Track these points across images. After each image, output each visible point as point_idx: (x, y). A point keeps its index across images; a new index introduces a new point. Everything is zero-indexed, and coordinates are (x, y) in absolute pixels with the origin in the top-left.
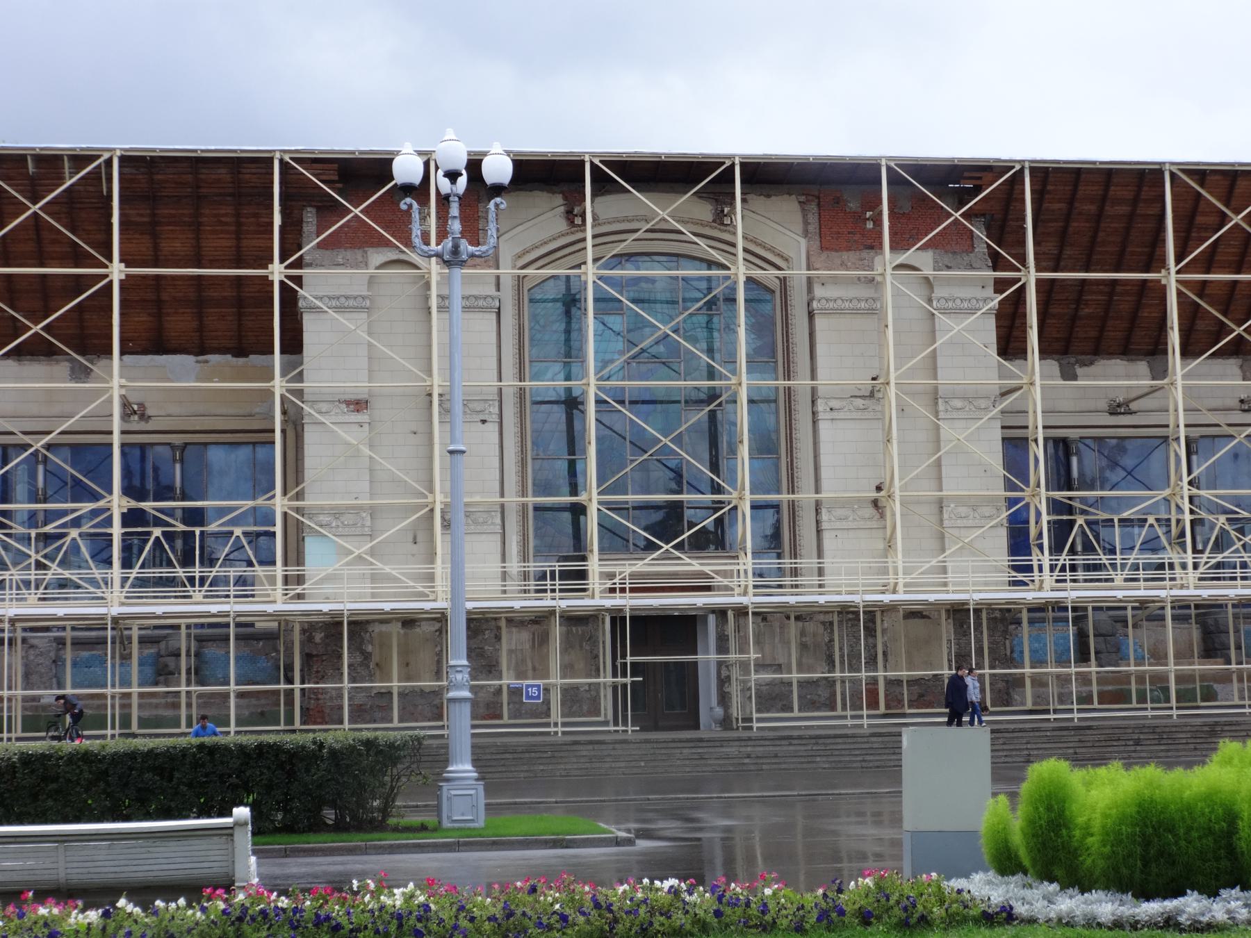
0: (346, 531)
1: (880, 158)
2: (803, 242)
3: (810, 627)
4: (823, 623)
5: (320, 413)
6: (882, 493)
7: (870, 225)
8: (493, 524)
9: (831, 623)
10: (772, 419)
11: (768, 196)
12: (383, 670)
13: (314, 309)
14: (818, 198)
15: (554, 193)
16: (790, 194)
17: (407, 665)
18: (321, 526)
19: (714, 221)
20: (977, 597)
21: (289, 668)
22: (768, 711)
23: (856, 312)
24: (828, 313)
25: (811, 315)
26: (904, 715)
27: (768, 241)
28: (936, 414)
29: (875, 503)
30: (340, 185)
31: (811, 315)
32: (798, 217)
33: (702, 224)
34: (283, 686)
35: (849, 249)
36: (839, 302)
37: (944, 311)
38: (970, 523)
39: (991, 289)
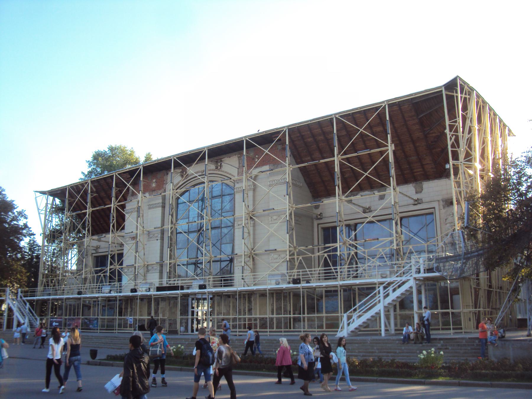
1: (242, 138)
11: (230, 157)
12: (322, 312)
21: (290, 312)
27: (229, 172)
33: (213, 170)
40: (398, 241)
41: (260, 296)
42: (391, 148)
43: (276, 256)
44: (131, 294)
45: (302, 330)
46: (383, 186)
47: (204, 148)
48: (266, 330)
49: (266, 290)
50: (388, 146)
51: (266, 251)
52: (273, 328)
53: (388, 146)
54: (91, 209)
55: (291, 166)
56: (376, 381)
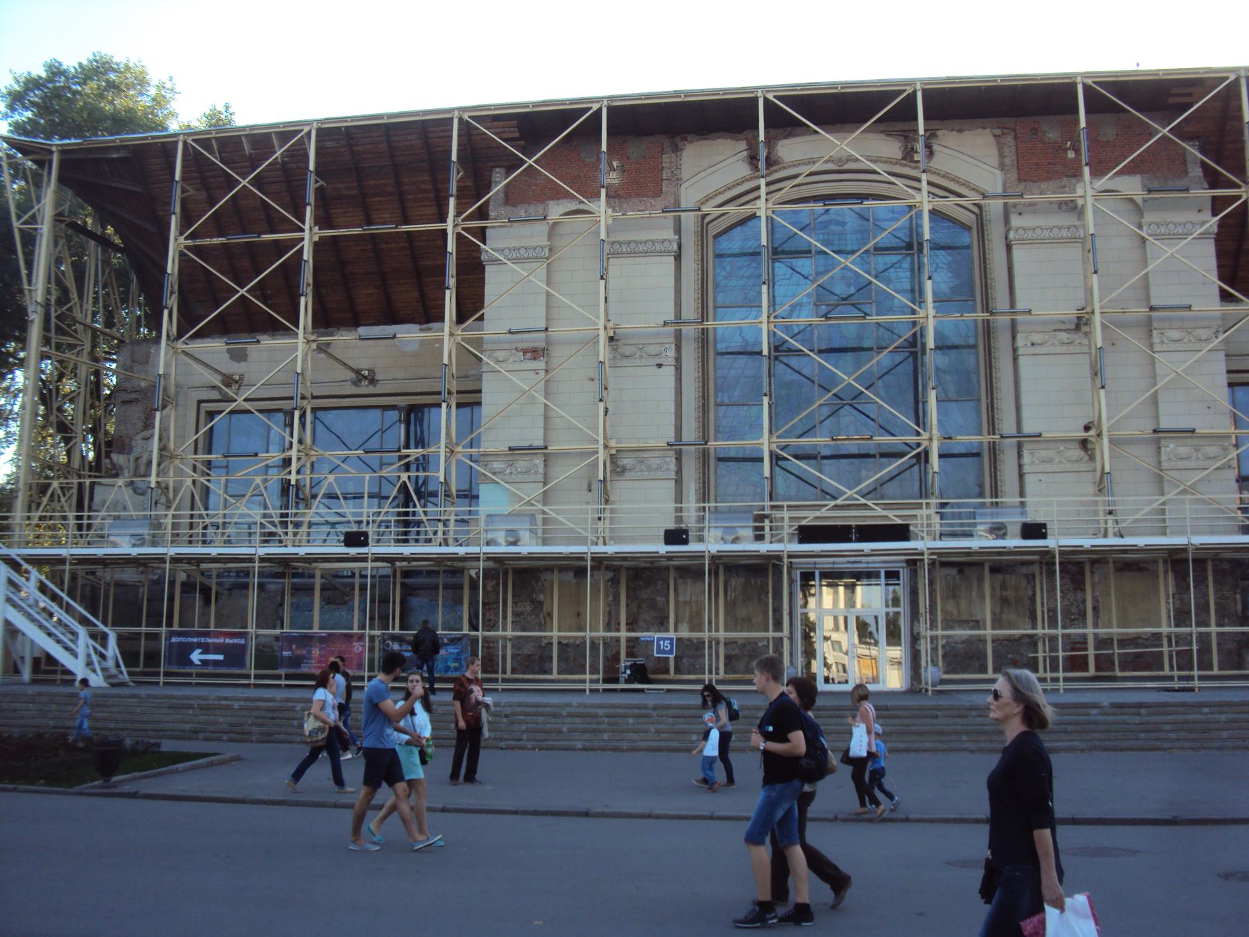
0: (520, 478)
1: (1075, 75)
2: (998, 173)
3: (1012, 580)
4: (1026, 576)
5: (497, 361)
6: (1092, 432)
7: (1071, 154)
8: (668, 470)
9: (1034, 575)
10: (972, 359)
11: (960, 131)
13: (496, 261)
14: (1014, 130)
15: (737, 140)
16: (985, 128)
17: (579, 615)
18: (494, 474)
19: (903, 158)
20: (1197, 540)
22: (964, 672)
23: (1059, 241)
24: (1023, 242)
25: (1009, 248)
26: (1114, 679)
27: (963, 176)
28: (1151, 346)
29: (1084, 443)
30: (523, 143)
31: (1009, 248)
32: (994, 151)
34: (771, 634)
35: (1049, 179)
36: (1038, 231)
37: (1158, 237)
38: (1193, 464)
39: (1209, 212)
40: (301, 463)
41: (1118, 570)
42: (311, 237)
43: (1183, 451)
44: (663, 549)
45: (500, 676)
46: (288, 329)
47: (911, 83)
48: (582, 677)
49: (582, 559)
50: (303, 230)
51: (510, 449)
52: (1210, 668)
53: (303, 230)
54: (318, 233)
55: (316, 229)
56: (61, 793)
